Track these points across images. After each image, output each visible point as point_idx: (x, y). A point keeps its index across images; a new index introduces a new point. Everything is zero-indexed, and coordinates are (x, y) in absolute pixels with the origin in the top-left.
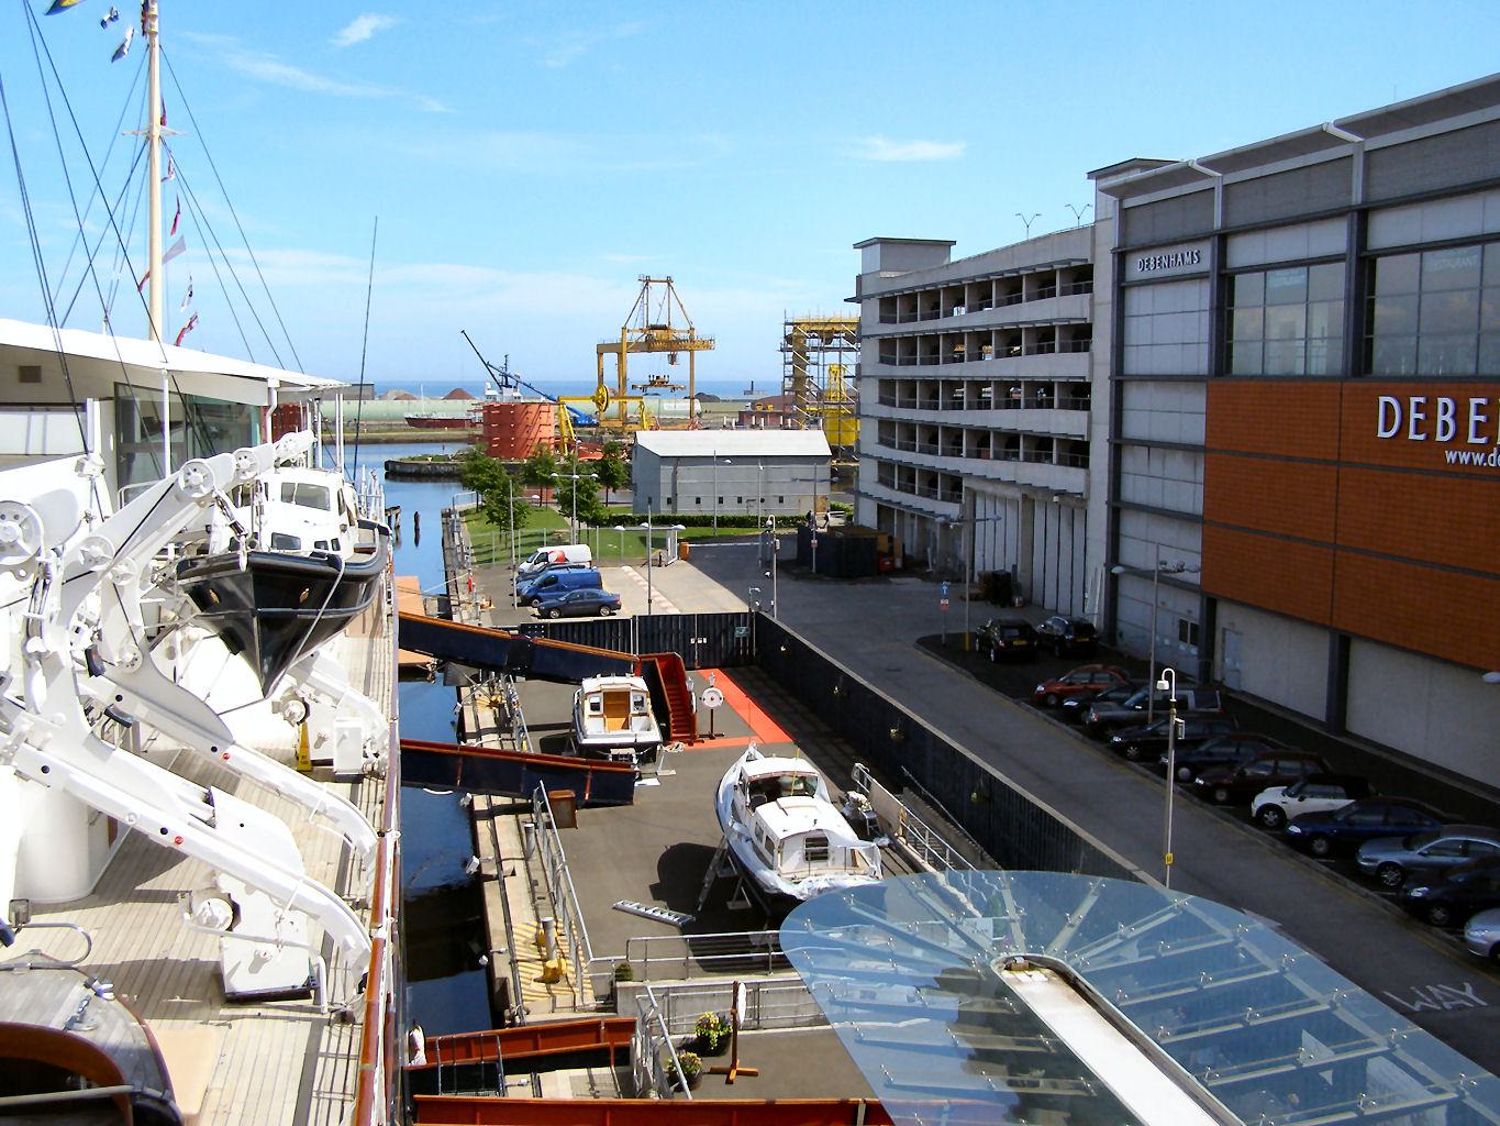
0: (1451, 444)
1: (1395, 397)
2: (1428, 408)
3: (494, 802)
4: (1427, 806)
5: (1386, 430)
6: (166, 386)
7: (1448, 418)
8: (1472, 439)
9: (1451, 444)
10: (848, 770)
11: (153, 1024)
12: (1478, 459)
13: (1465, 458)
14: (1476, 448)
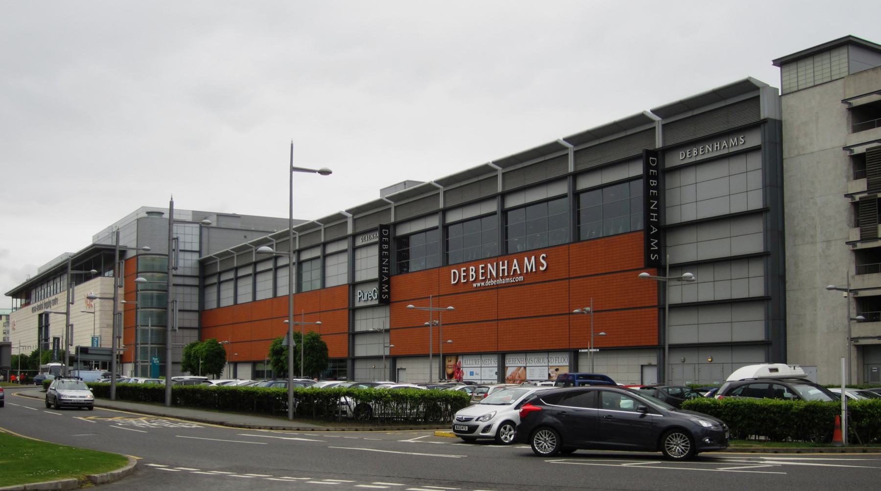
0: (474, 282)
1: (456, 269)
2: (466, 271)
3: (841, 391)
4: (702, 448)
5: (454, 281)
6: (379, 423)
7: (473, 273)
8: (481, 278)
9: (474, 282)
10: (714, 404)
11: (727, 380)
12: (483, 284)
13: (479, 285)
14: (482, 280)
